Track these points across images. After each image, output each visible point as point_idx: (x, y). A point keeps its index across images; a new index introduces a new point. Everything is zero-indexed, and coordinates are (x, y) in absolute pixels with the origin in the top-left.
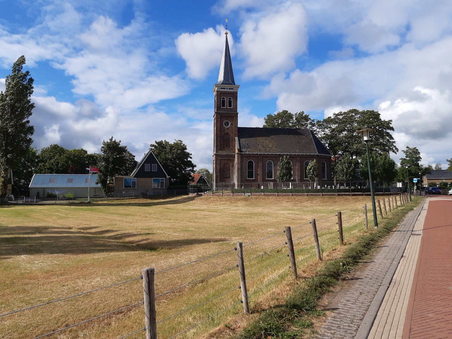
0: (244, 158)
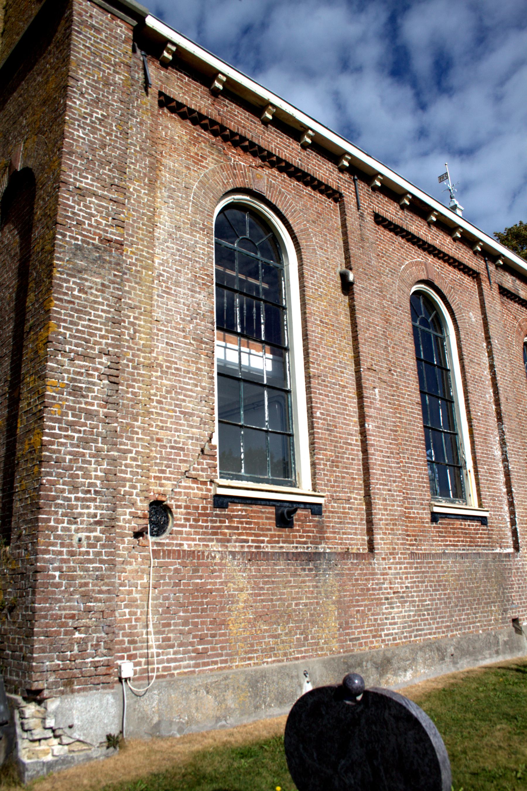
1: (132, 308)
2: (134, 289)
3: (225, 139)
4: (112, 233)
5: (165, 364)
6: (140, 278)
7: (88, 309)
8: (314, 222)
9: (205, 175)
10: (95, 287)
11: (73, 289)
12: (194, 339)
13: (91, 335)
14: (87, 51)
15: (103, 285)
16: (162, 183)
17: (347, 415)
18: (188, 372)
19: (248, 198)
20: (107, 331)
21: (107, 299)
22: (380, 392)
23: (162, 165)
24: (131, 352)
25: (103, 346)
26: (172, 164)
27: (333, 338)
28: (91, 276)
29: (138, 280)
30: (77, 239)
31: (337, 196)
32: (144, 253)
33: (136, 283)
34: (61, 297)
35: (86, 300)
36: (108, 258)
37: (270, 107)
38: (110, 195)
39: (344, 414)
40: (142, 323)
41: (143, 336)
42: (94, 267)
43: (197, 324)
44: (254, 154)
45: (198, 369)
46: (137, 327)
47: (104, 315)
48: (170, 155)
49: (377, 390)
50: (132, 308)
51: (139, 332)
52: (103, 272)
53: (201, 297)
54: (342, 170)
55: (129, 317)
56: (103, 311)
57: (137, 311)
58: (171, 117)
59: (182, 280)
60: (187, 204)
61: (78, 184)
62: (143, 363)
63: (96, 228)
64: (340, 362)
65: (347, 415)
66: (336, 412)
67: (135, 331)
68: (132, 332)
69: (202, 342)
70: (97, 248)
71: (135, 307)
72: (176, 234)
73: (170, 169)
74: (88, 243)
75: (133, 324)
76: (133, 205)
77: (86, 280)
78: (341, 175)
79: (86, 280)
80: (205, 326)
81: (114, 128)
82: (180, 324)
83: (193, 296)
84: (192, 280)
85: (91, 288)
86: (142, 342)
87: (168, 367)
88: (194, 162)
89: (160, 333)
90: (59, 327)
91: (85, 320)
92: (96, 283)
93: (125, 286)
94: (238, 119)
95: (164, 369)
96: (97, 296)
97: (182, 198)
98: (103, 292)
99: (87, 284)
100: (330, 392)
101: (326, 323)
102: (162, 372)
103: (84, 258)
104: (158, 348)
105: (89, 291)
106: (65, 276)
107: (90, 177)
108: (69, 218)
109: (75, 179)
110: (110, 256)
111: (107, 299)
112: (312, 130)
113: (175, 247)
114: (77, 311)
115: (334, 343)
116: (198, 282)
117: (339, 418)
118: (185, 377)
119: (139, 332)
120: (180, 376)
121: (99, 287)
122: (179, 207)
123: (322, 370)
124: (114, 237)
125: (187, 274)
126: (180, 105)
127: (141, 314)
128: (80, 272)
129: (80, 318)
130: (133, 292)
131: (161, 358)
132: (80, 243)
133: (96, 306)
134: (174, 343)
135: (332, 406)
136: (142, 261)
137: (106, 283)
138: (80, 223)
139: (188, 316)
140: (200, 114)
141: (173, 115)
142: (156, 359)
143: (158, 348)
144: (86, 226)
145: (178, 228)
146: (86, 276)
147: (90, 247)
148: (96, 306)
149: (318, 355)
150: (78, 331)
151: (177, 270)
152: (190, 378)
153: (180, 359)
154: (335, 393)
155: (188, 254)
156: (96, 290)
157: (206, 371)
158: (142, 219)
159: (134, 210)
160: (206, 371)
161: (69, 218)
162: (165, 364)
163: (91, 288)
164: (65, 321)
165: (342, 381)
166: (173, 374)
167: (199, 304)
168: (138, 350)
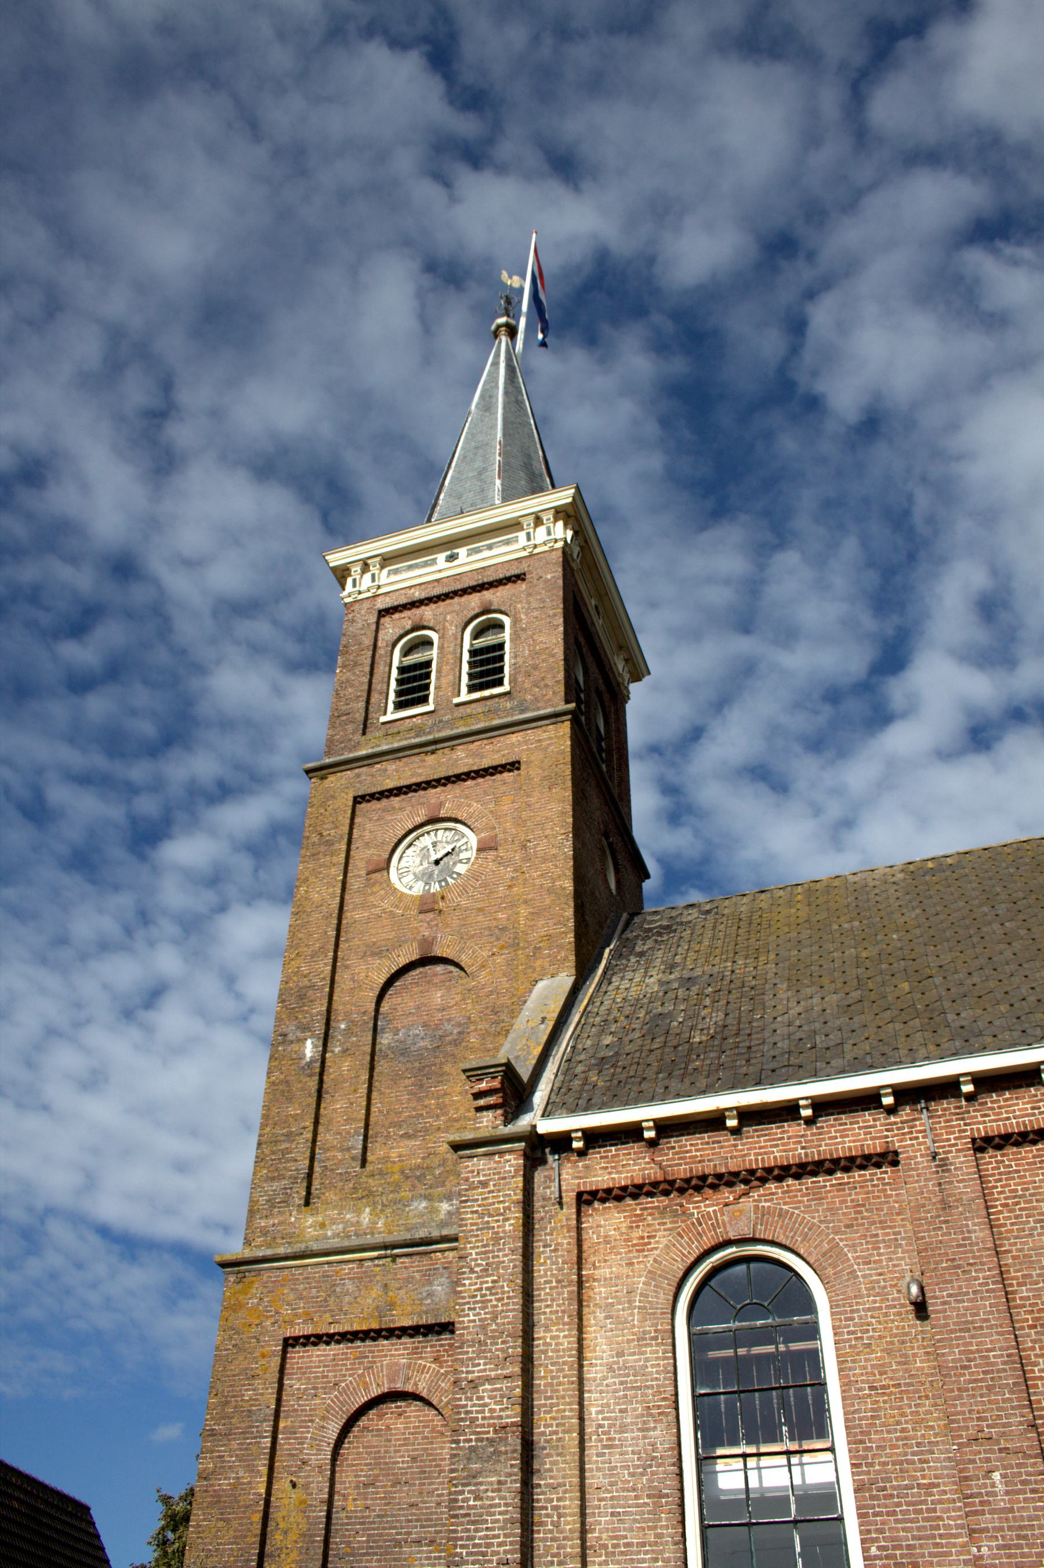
0: (607, 1222)
1: (554, 1488)
2: (555, 1463)
3: (682, 1191)
4: (508, 1417)
5: (610, 1543)
6: (563, 1447)
7: (485, 1517)
8: (847, 1226)
9: (655, 1261)
10: (490, 1487)
11: (468, 1499)
12: (649, 1496)
13: (489, 1545)
14: (475, 1216)
15: (499, 1482)
16: (596, 1305)
17: (941, 1536)
18: (643, 1544)
19: (734, 1249)
20: (505, 1536)
21: (505, 1498)
22: (1003, 1476)
23: (595, 1280)
24: (555, 1544)
25: (502, 1556)
26: (608, 1271)
27: (900, 1408)
28: (487, 1477)
29: (560, 1450)
30: (471, 1440)
31: (890, 1158)
32: (567, 1413)
33: (558, 1455)
34: (457, 1512)
35: (482, 1507)
36: (503, 1449)
37: (727, 1114)
38: (504, 1372)
39: (934, 1537)
40: (567, 1503)
41: (569, 1519)
42: (488, 1466)
43: (653, 1473)
44: (730, 1184)
45: (658, 1536)
46: (562, 1511)
47: (501, 1517)
48: (605, 1261)
49: (996, 1476)
50: (554, 1488)
51: (565, 1515)
52: (498, 1467)
53: (658, 1432)
54: (891, 1110)
55: (552, 1500)
56: (500, 1513)
57: (560, 1489)
58: (604, 1208)
59: (629, 1420)
60: (632, 1314)
61: (470, 1376)
62: (570, 1554)
63: (492, 1418)
64: (918, 1444)
65: (941, 1536)
66: (914, 1538)
67: (559, 1516)
68: (555, 1518)
69: (661, 1496)
70: (491, 1441)
71: (559, 1485)
72: (618, 1363)
73: (605, 1279)
74: (481, 1440)
75: (556, 1508)
76: (551, 1358)
77: (481, 1484)
78: (893, 1119)
79: (481, 1484)
80: (665, 1472)
81: (506, 1289)
82: (629, 1481)
83: (644, 1437)
84: (643, 1415)
85: (487, 1490)
86: (568, 1527)
87: (615, 1546)
88: (638, 1251)
89: (603, 1503)
90: (455, 1546)
91: (482, 1530)
92: (491, 1483)
93: (545, 1463)
94: (67, 1530)
95: (610, 1549)
96: (493, 1498)
97: (623, 1310)
98: (499, 1490)
99: (482, 1488)
100: (899, 1504)
101: (883, 1387)
102: (607, 1555)
103: (479, 1459)
104: (600, 1524)
105: (484, 1495)
106: (460, 1488)
107: (482, 1362)
108: (462, 1420)
109: (468, 1372)
110: (505, 1446)
111: (505, 1498)
112: (802, 1098)
113: (617, 1380)
114: (473, 1523)
115: (903, 1415)
116: (652, 1415)
117: (921, 1546)
118: (639, 1553)
119: (565, 1515)
120: (632, 1553)
121: (495, 1486)
122: (620, 1322)
123: (878, 1472)
124: (509, 1420)
125: (635, 1409)
126: (608, 1191)
127: (565, 1492)
128: (474, 1477)
129: (476, 1530)
130: (554, 1467)
131: (604, 1536)
132: (474, 1443)
133: (493, 1510)
134: (621, 1510)
135: (904, 1529)
136: (564, 1425)
137: (502, 1478)
138: (473, 1420)
139: (638, 1466)
140: (635, 1186)
141: (607, 1205)
142: (599, 1538)
143: (600, 1524)
144: (480, 1421)
145: (621, 1354)
146: (481, 1480)
147: (485, 1443)
148: (493, 1510)
149: (867, 1449)
150: (475, 1546)
151: (621, 1411)
152: (646, 1552)
153: (631, 1530)
154: (908, 1504)
155: (636, 1381)
156: (493, 1491)
157: (669, 1536)
158: (563, 1370)
159: (552, 1364)
160: (669, 1536)
161: (462, 1420)
162: (610, 1543)
163: (487, 1490)
164: (461, 1538)
165: (924, 1477)
166: (622, 1553)
167: (653, 1445)
168: (564, 1539)
